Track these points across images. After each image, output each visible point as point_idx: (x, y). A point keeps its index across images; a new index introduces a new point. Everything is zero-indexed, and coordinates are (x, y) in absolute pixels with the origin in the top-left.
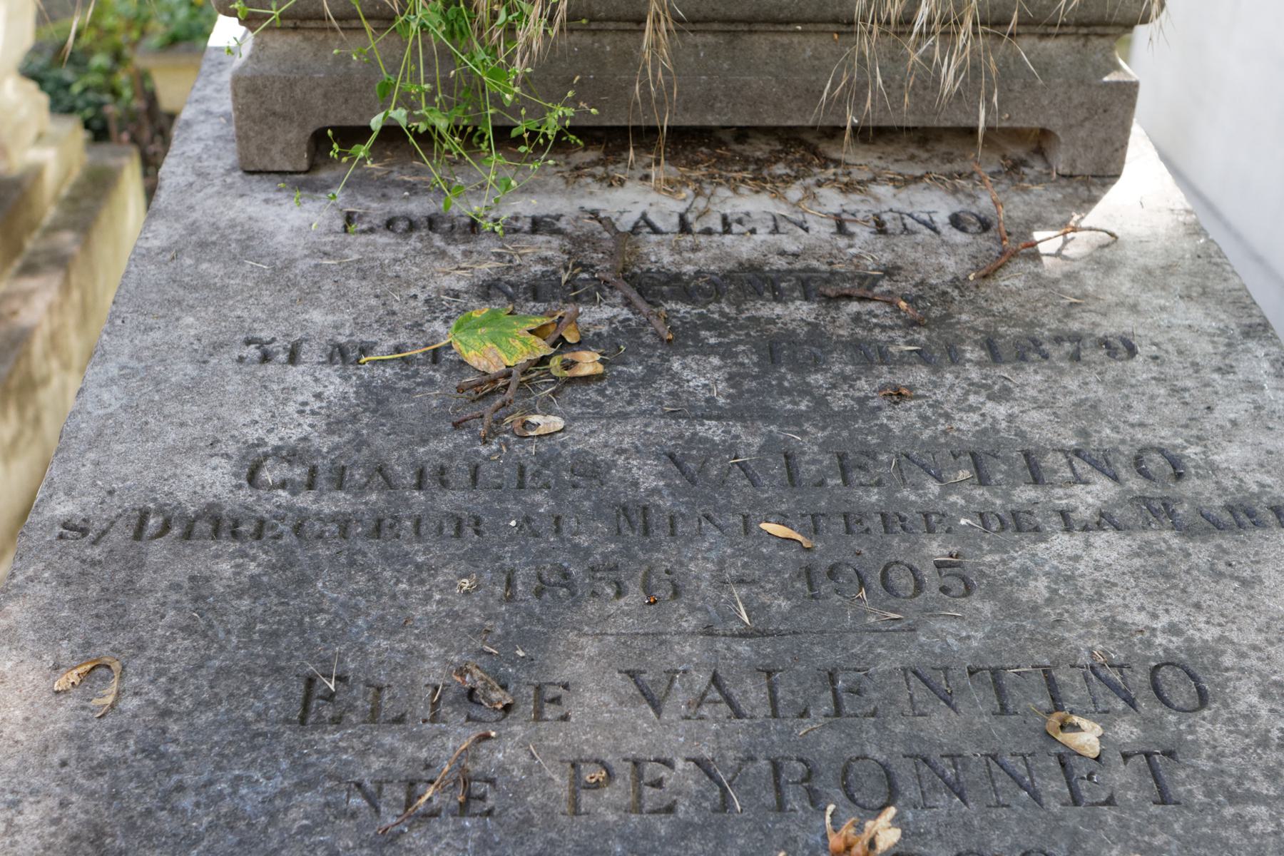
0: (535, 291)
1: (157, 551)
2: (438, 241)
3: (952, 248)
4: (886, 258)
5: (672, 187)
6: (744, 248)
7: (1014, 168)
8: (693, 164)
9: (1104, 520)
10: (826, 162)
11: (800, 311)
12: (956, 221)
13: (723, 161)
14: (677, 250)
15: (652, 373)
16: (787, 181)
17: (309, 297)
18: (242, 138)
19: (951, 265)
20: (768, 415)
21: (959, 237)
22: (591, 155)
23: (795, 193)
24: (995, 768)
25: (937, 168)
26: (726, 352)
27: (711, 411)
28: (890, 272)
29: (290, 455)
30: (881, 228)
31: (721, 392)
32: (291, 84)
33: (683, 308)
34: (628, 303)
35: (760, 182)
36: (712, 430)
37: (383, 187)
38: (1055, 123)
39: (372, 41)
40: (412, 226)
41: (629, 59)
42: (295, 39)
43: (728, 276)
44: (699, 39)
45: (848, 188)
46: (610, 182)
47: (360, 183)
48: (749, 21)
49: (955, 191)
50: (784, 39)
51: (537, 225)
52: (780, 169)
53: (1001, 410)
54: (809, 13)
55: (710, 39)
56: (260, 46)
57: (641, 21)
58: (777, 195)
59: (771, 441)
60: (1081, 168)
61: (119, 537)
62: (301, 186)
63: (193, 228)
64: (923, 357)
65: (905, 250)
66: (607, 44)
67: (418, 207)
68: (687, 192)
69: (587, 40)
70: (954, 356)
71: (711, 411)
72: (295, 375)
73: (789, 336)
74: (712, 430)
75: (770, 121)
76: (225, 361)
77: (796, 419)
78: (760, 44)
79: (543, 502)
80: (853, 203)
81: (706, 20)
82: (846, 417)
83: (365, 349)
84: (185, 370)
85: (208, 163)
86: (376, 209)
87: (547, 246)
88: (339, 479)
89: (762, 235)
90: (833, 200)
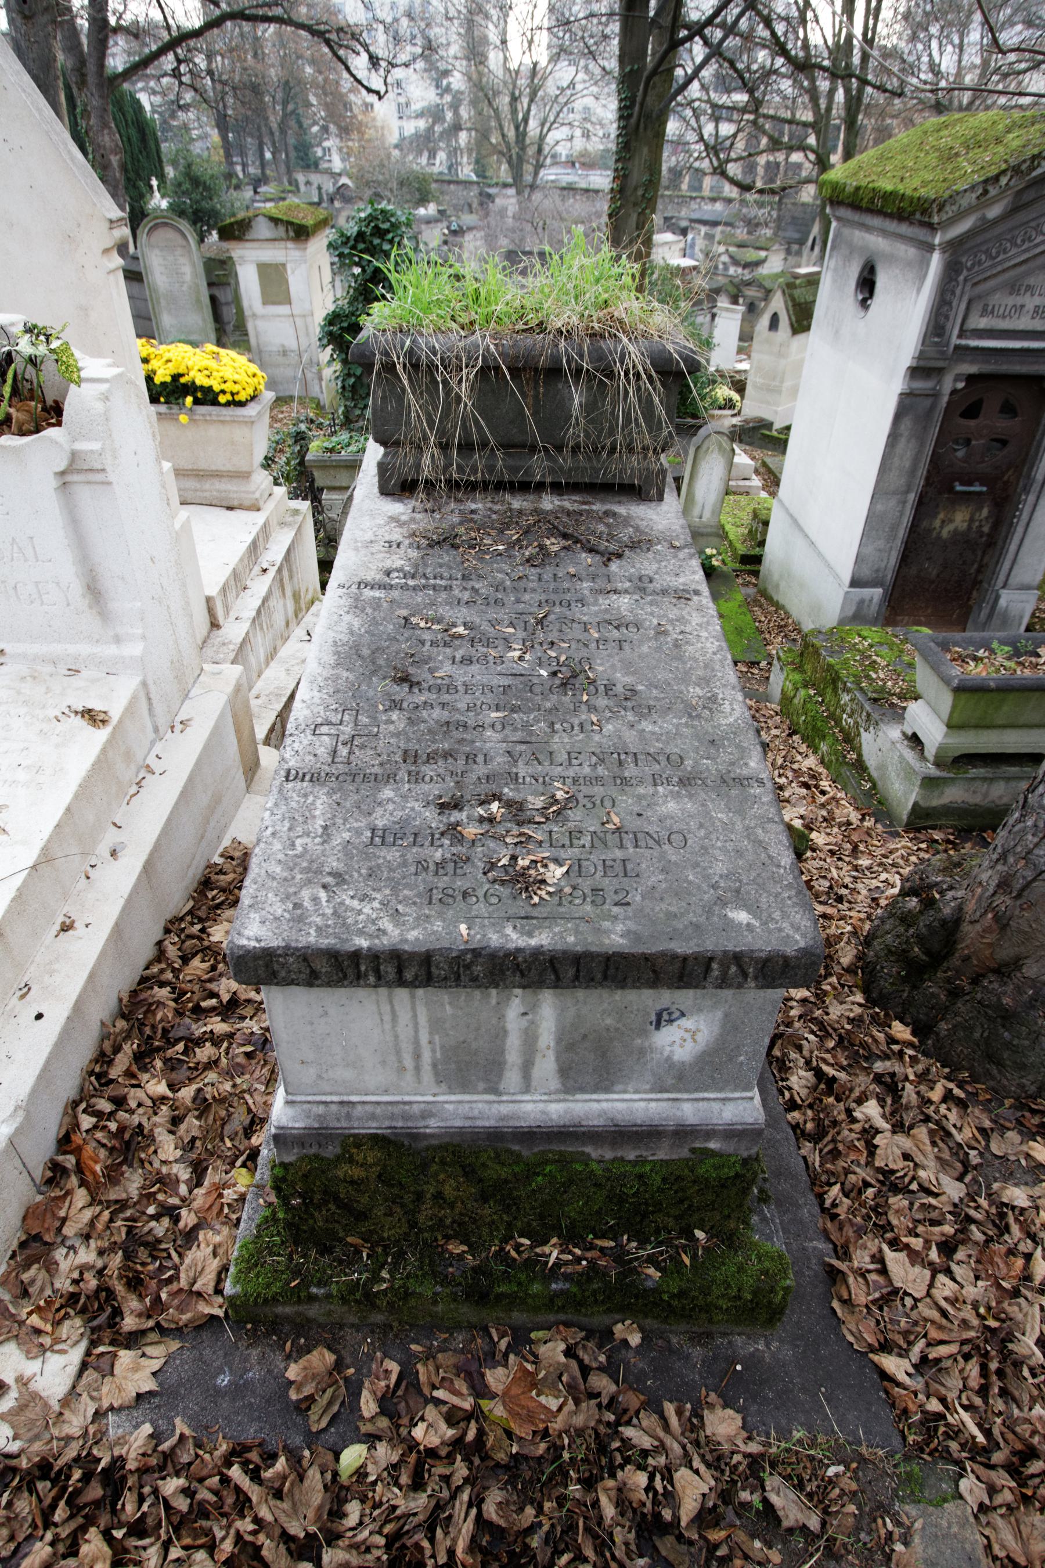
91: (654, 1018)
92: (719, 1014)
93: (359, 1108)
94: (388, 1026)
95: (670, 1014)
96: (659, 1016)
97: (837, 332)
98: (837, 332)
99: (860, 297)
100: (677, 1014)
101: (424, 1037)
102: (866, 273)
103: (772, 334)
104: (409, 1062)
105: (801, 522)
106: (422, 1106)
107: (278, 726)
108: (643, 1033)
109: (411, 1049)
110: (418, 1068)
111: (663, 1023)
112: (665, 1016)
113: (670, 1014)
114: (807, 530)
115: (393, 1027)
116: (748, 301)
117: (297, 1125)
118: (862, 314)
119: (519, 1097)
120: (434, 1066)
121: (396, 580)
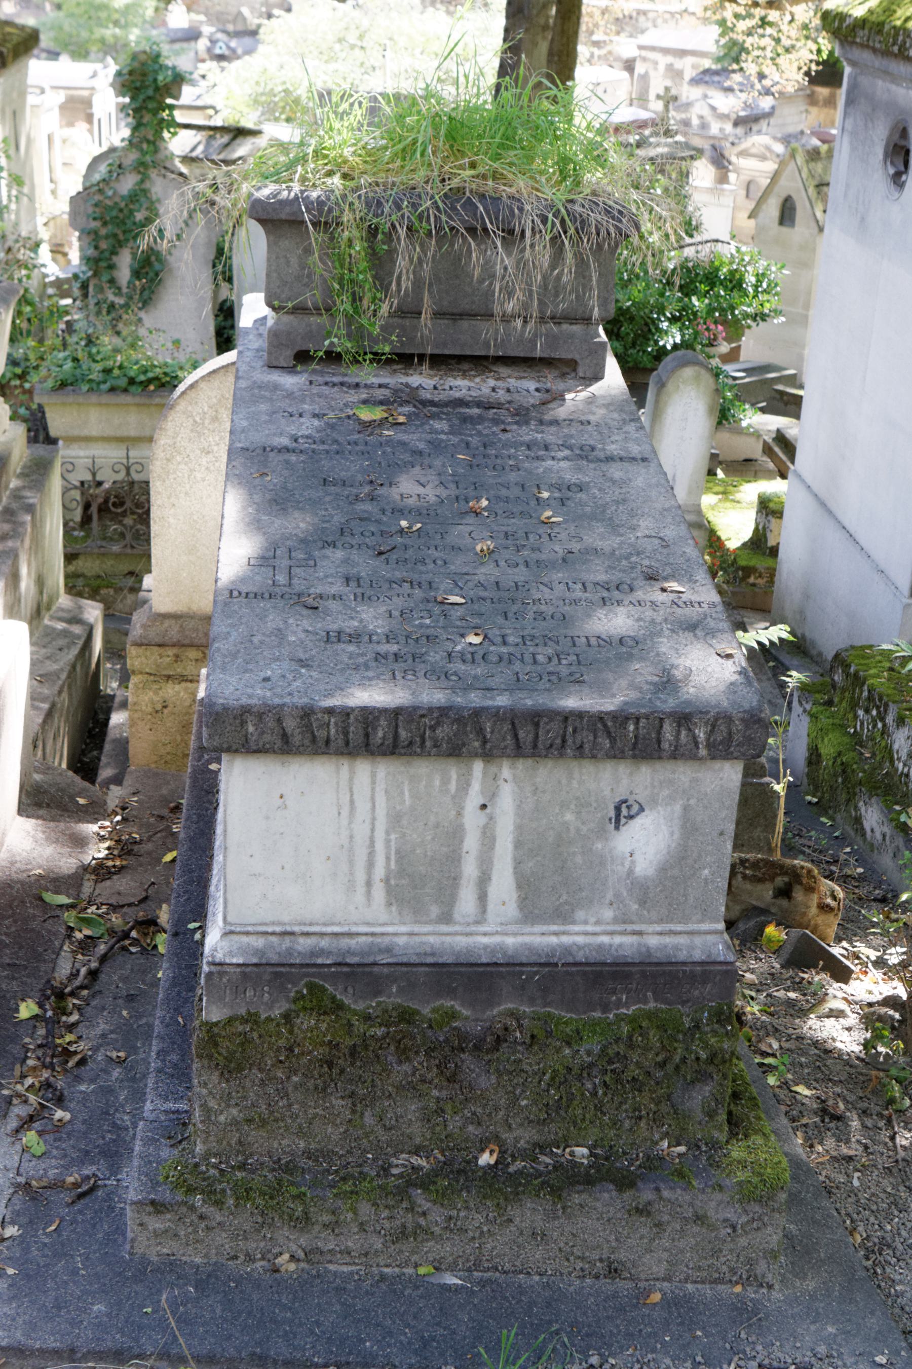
0: (381, 403)
1: (272, 454)
2: (345, 389)
3: (534, 397)
4: (509, 399)
5: (431, 377)
6: (457, 395)
7: (563, 375)
8: (439, 370)
9: (565, 458)
10: (491, 371)
11: (476, 411)
12: (537, 390)
13: (451, 370)
14: (432, 394)
15: (422, 424)
16: (475, 376)
17: (303, 401)
18: (270, 353)
19: (532, 401)
20: (461, 434)
21: (537, 394)
22: (399, 367)
23: (478, 380)
24: (599, 725)
25: (533, 374)
26: (449, 420)
27: (442, 432)
28: (509, 402)
29: (307, 437)
30: (508, 390)
31: (446, 428)
32: (289, 333)
33: (434, 409)
34: (415, 406)
35: (464, 376)
36: (443, 437)
37: (322, 373)
38: (577, 357)
39: (324, 319)
40: (334, 385)
41: (415, 328)
42: (291, 317)
43: (451, 402)
44: (442, 322)
45: (497, 379)
46: (407, 375)
47: (314, 371)
48: (461, 315)
49: (539, 381)
50: (474, 322)
51: (380, 386)
52: (473, 373)
53: (540, 436)
54: (482, 312)
55: (446, 321)
56: (278, 319)
57: (420, 313)
58: (470, 380)
59: (462, 440)
60: (588, 375)
61: (259, 451)
62: (290, 372)
63: (255, 382)
64: (516, 423)
65: (516, 397)
66: (407, 322)
67: (336, 379)
68: (437, 378)
69: (400, 321)
70: (527, 423)
71: (442, 432)
72: (302, 420)
73: (471, 417)
74: (443, 437)
75: (469, 353)
76: (279, 415)
77: (471, 436)
78: (465, 324)
79: (389, 450)
80: (499, 384)
81: (444, 314)
82: (487, 435)
83: (324, 415)
84: (265, 418)
85: (254, 364)
86: (321, 379)
87: (387, 392)
88: (323, 443)
89: (464, 391)
90: (492, 382)
91: (612, 814)
92: (678, 808)
93: (301, 940)
94: (345, 822)
95: (629, 807)
96: (618, 809)
97: (863, 219)
98: (863, 219)
99: (891, 171)
100: (635, 808)
101: (380, 836)
102: (896, 137)
103: (784, 230)
104: (360, 876)
105: (834, 508)
106: (370, 939)
107: (41, 737)
108: (601, 833)
109: (365, 858)
110: (369, 884)
111: (623, 821)
112: (624, 812)
113: (629, 807)
114: (841, 517)
115: (350, 823)
116: (745, 178)
117: (235, 961)
118: (897, 195)
119: (473, 928)
120: (387, 880)
121: (303, 444)
